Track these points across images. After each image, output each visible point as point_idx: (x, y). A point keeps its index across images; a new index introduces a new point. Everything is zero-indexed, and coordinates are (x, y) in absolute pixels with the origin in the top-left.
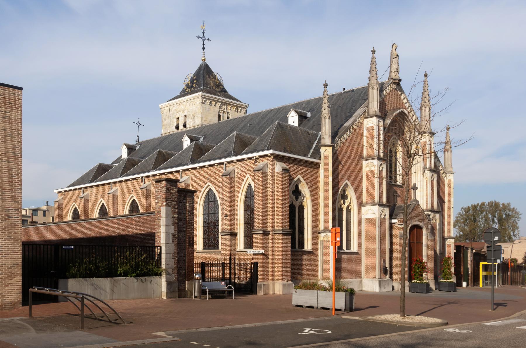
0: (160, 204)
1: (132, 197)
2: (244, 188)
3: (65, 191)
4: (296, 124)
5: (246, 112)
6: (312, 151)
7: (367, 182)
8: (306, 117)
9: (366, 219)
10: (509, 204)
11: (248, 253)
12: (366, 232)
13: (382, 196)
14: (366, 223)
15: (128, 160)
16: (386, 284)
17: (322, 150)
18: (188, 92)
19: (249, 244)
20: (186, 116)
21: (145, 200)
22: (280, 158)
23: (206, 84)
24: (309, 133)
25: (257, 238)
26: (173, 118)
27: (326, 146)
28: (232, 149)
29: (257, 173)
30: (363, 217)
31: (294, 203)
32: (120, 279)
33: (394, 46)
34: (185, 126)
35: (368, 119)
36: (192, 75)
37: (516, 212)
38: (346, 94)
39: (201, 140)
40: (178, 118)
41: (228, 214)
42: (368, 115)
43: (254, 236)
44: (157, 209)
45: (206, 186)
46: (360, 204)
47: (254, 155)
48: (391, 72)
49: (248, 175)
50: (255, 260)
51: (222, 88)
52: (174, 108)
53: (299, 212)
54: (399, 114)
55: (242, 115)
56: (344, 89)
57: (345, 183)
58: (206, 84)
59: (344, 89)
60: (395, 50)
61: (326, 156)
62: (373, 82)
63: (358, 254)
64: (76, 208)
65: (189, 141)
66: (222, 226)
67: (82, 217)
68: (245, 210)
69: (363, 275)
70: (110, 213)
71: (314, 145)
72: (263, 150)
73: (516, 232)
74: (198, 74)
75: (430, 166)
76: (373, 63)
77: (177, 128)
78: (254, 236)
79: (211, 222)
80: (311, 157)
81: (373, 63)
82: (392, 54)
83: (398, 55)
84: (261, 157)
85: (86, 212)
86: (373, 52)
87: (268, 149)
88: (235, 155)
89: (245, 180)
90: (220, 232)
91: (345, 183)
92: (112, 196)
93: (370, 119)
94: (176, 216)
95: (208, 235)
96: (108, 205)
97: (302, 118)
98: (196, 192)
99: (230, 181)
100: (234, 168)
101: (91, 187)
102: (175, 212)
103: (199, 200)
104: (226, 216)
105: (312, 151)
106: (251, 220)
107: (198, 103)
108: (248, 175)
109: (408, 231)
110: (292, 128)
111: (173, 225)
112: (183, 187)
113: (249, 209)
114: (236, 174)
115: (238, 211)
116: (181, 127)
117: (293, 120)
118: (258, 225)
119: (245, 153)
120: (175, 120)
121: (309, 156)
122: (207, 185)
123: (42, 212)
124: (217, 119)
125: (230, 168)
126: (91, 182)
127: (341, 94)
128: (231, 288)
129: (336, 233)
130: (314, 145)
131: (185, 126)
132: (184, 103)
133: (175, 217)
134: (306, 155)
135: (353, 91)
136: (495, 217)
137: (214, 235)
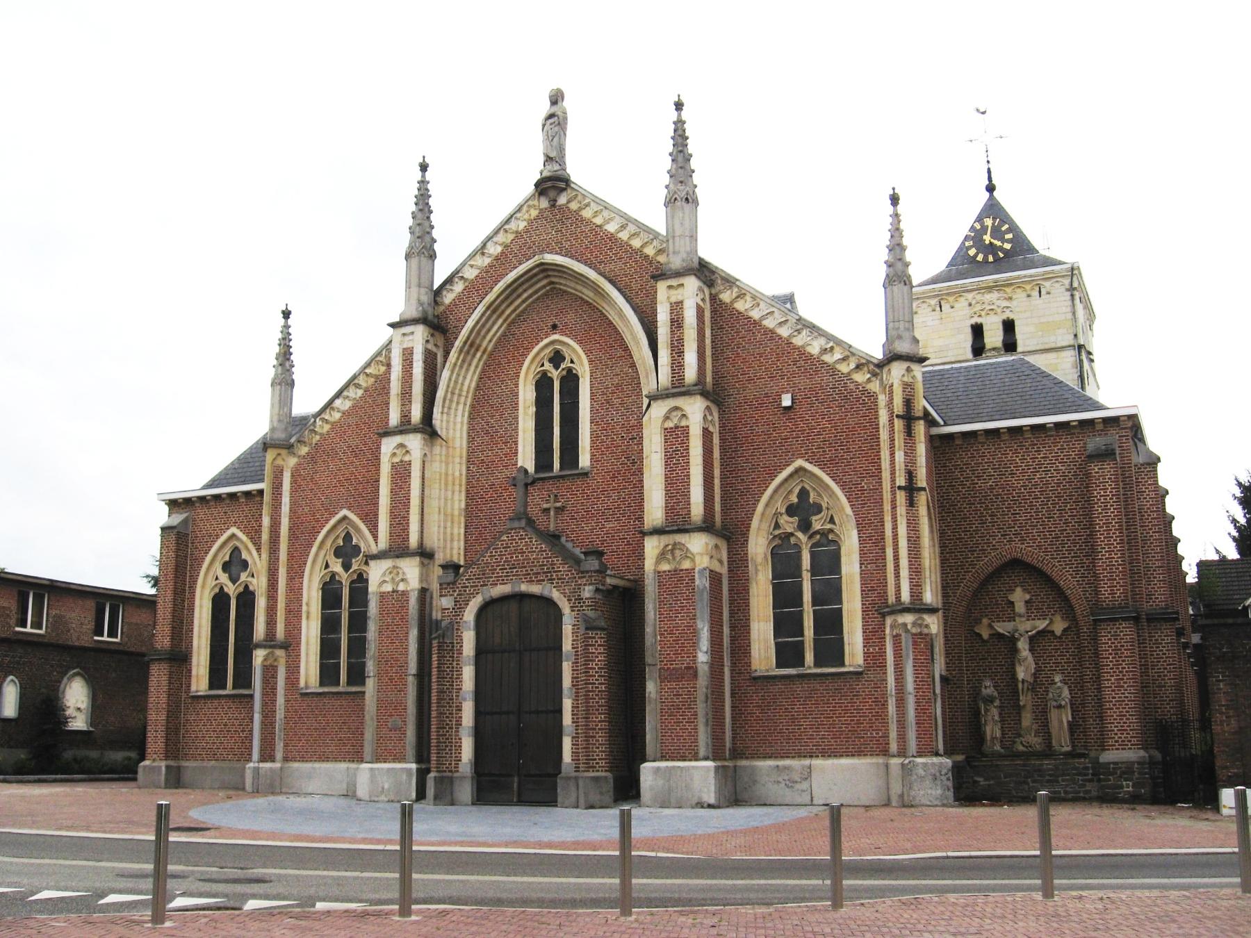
57: (229, 533)
122: (229, 533)
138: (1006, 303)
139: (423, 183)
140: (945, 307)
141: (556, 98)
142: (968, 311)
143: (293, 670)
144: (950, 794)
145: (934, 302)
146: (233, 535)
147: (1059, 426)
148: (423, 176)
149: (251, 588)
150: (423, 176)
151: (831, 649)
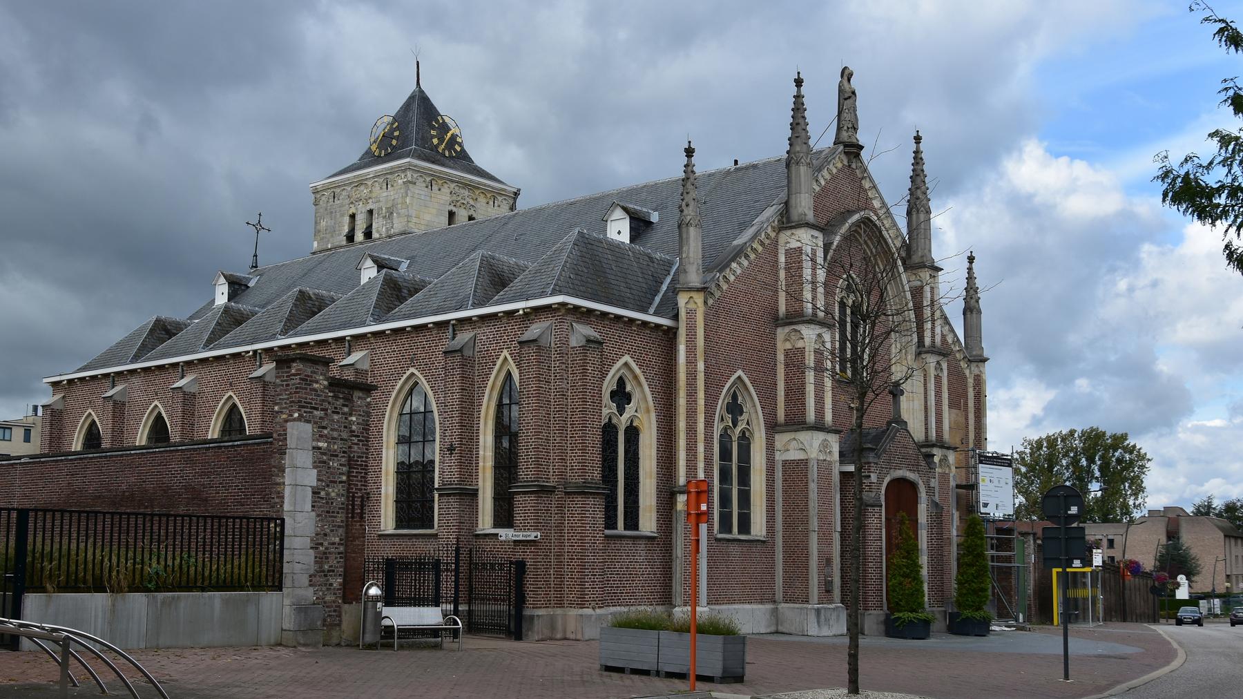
0: (284, 416)
1: (230, 397)
2: (494, 381)
3: (70, 382)
4: (625, 238)
5: (512, 208)
6: (657, 299)
7: (786, 375)
8: (649, 224)
9: (785, 462)
10: (1124, 437)
11: (503, 538)
12: (785, 491)
13: (823, 408)
14: (784, 472)
15: (226, 310)
16: (834, 617)
17: (682, 300)
18: (379, 156)
19: (504, 517)
20: (371, 212)
21: (259, 407)
22: (582, 313)
23: (424, 140)
24: (651, 259)
25: (524, 505)
26: (342, 215)
27: (690, 289)
28: (470, 288)
29: (525, 349)
30: (779, 457)
31: (614, 421)
32: (179, 597)
33: (847, 72)
34: (368, 234)
35: (789, 233)
36: (387, 120)
37: (1139, 455)
38: (740, 174)
39: (403, 267)
40: (353, 217)
41: (456, 444)
42: (789, 220)
43: (518, 498)
44: (278, 427)
45: (405, 376)
46: (773, 427)
47: (520, 305)
48: (839, 129)
49: (505, 353)
50: (519, 556)
51: (458, 149)
52: (344, 193)
53: (627, 441)
54: (857, 224)
55: (504, 210)
56: (736, 162)
57: (736, 375)
58: (424, 140)
59: (736, 162)
60: (849, 80)
61: (691, 313)
62: (798, 149)
63: (765, 544)
64: (159, 418)
65: (375, 269)
66: (442, 472)
67: (106, 444)
68: (498, 437)
69: (779, 595)
70: (175, 436)
71: (664, 287)
72: (542, 294)
73: (1140, 500)
74: (402, 118)
75: (933, 342)
76: (799, 107)
77: (350, 238)
78: (518, 498)
79: (417, 462)
80: (656, 314)
81: (799, 107)
82: (841, 91)
83: (854, 93)
84: (536, 310)
85: (118, 432)
86: (799, 82)
87: (552, 294)
88: (475, 306)
89: (499, 362)
90: (436, 486)
91: (736, 375)
92: (181, 395)
93: (793, 231)
94: (1016, 456)
95: (409, 494)
96: (171, 416)
97: (640, 226)
98: (368, 389)
99: (463, 366)
100: (472, 334)
101: (132, 372)
102: (321, 436)
103: (388, 409)
104: (451, 449)
105: (657, 299)
106: (510, 459)
107: (400, 181)
108: (505, 353)
109: (883, 492)
110: (615, 247)
111: (315, 467)
112: (351, 378)
113: (503, 430)
114: (477, 349)
115: (481, 438)
116: (359, 236)
117: (619, 230)
118: (526, 472)
119: (296, 335)
120: (347, 219)
121: (652, 310)
122: (408, 373)
123: (22, 430)
124: (445, 219)
125: (464, 337)
126: (135, 359)
127: (728, 172)
128: (456, 623)
129: (698, 493)
130: (664, 287)
131: (368, 234)
132: (370, 183)
133: (320, 448)
134: (644, 310)
135: (754, 166)
136: (1094, 462)
137: (423, 493)
138: (472, 202)
139: (798, 97)
140: (435, 187)
141: (846, 74)
142: (448, 198)
143: (710, 530)
144: (882, 627)
145: (428, 179)
146: (413, 374)
147: (416, 328)
148: (799, 91)
149: (1028, 422)
150: (799, 91)
151: (745, 525)
